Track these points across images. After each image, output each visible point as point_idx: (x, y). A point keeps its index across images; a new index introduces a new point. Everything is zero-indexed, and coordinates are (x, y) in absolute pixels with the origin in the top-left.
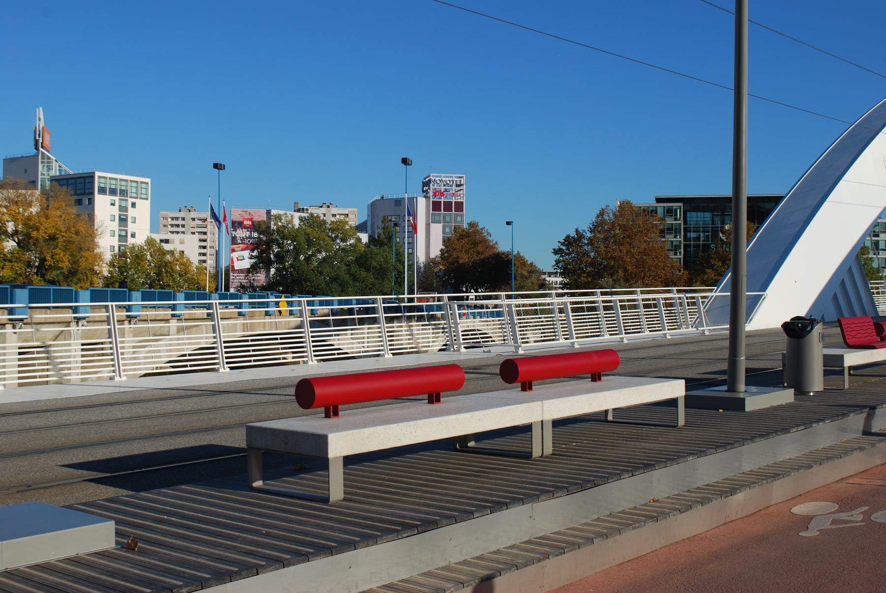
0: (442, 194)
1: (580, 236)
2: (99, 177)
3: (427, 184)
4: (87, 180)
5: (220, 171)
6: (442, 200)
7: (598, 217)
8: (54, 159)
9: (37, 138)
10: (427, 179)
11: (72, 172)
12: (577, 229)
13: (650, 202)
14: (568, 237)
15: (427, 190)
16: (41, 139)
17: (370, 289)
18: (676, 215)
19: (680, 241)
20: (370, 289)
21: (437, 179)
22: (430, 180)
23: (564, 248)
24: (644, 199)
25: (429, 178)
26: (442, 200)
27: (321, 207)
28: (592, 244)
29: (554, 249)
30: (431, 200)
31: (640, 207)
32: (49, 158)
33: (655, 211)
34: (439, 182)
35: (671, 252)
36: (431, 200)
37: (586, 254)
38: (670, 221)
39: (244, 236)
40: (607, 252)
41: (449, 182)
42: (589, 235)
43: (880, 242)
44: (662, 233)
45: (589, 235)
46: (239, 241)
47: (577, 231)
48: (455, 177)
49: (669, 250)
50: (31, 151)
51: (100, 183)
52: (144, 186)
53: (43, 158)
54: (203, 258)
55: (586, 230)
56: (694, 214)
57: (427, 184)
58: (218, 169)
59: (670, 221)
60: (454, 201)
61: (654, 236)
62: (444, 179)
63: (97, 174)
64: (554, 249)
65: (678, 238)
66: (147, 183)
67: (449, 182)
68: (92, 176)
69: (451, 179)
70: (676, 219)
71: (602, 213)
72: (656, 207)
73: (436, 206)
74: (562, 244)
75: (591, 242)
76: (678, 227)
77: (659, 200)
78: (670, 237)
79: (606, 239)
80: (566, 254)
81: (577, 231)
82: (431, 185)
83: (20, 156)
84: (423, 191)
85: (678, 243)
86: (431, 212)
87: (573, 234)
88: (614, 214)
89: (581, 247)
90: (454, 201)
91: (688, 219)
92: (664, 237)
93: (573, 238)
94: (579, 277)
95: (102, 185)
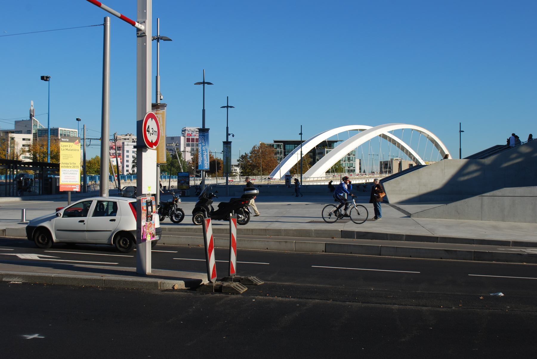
0: (191, 135)
1: (246, 155)
2: (60, 130)
3: (184, 131)
4: (55, 131)
5: (79, 121)
6: (191, 138)
7: (253, 149)
8: (38, 121)
9: (31, 113)
10: (184, 129)
11: (45, 128)
12: (245, 153)
13: (272, 142)
14: (242, 155)
15: (184, 133)
16: (33, 113)
17: (175, 174)
18: (281, 147)
19: (282, 157)
20: (175, 174)
21: (189, 129)
22: (186, 129)
23: (241, 159)
24: (270, 141)
25: (185, 129)
26: (191, 138)
27: (126, 135)
28: (251, 158)
29: (237, 160)
30: (186, 137)
31: (268, 144)
32: (36, 121)
33: (273, 146)
34: (189, 130)
35: (279, 161)
36: (186, 137)
37: (248, 161)
38: (278, 149)
39: (113, 152)
40: (256, 161)
41: (193, 130)
42: (250, 155)
43: (351, 157)
44: (276, 154)
45: (250, 155)
46: (112, 155)
47: (245, 153)
48: (196, 129)
49: (278, 160)
50: (28, 118)
51: (60, 132)
52: (75, 133)
53: (34, 121)
54: (72, 164)
55: (249, 153)
56: (288, 146)
57: (184, 131)
58: (78, 121)
59: (278, 149)
60: (195, 138)
61: (273, 155)
62: (191, 129)
63: (60, 129)
64: (237, 160)
65: (281, 156)
66: (76, 132)
67: (193, 130)
68: (57, 130)
69: (194, 129)
70: (280, 149)
71: (254, 147)
72: (274, 144)
73: (188, 140)
74: (241, 158)
75: (250, 158)
76: (281, 152)
77: (275, 142)
78: (278, 155)
79: (255, 156)
80: (242, 162)
81: (245, 153)
82: (186, 131)
83: (21, 120)
84: (182, 134)
85: (281, 157)
86: (186, 142)
87: (244, 154)
88: (258, 148)
89: (247, 159)
90: (195, 138)
91: (286, 148)
92: (276, 155)
93: (244, 156)
94: (246, 169)
95: (61, 133)
